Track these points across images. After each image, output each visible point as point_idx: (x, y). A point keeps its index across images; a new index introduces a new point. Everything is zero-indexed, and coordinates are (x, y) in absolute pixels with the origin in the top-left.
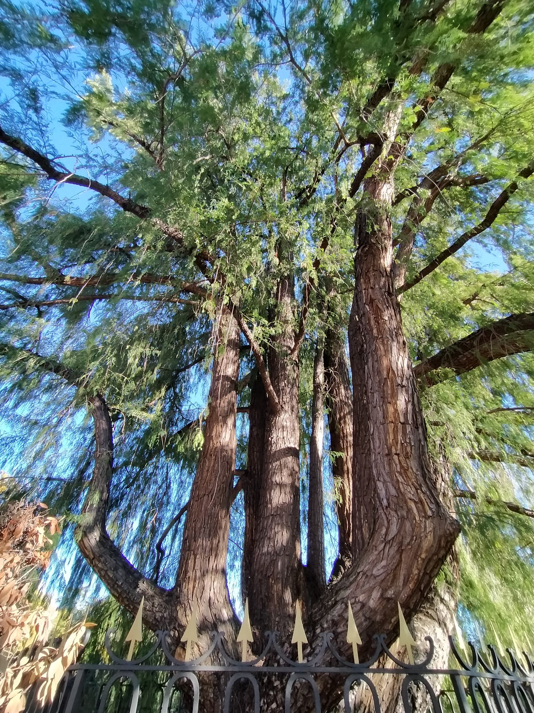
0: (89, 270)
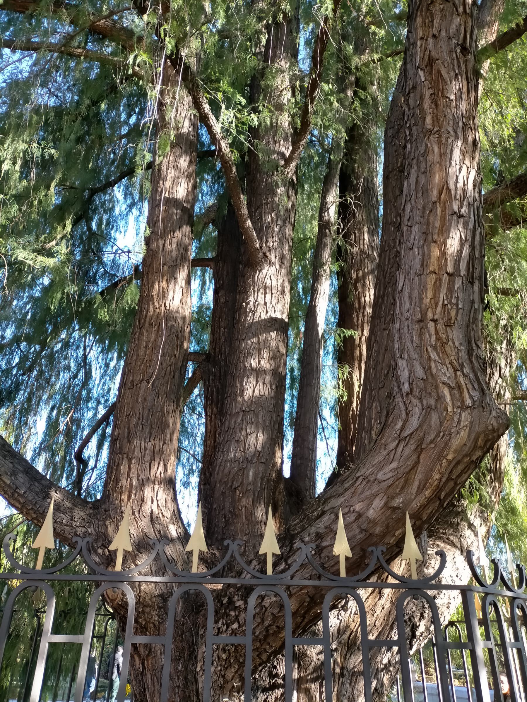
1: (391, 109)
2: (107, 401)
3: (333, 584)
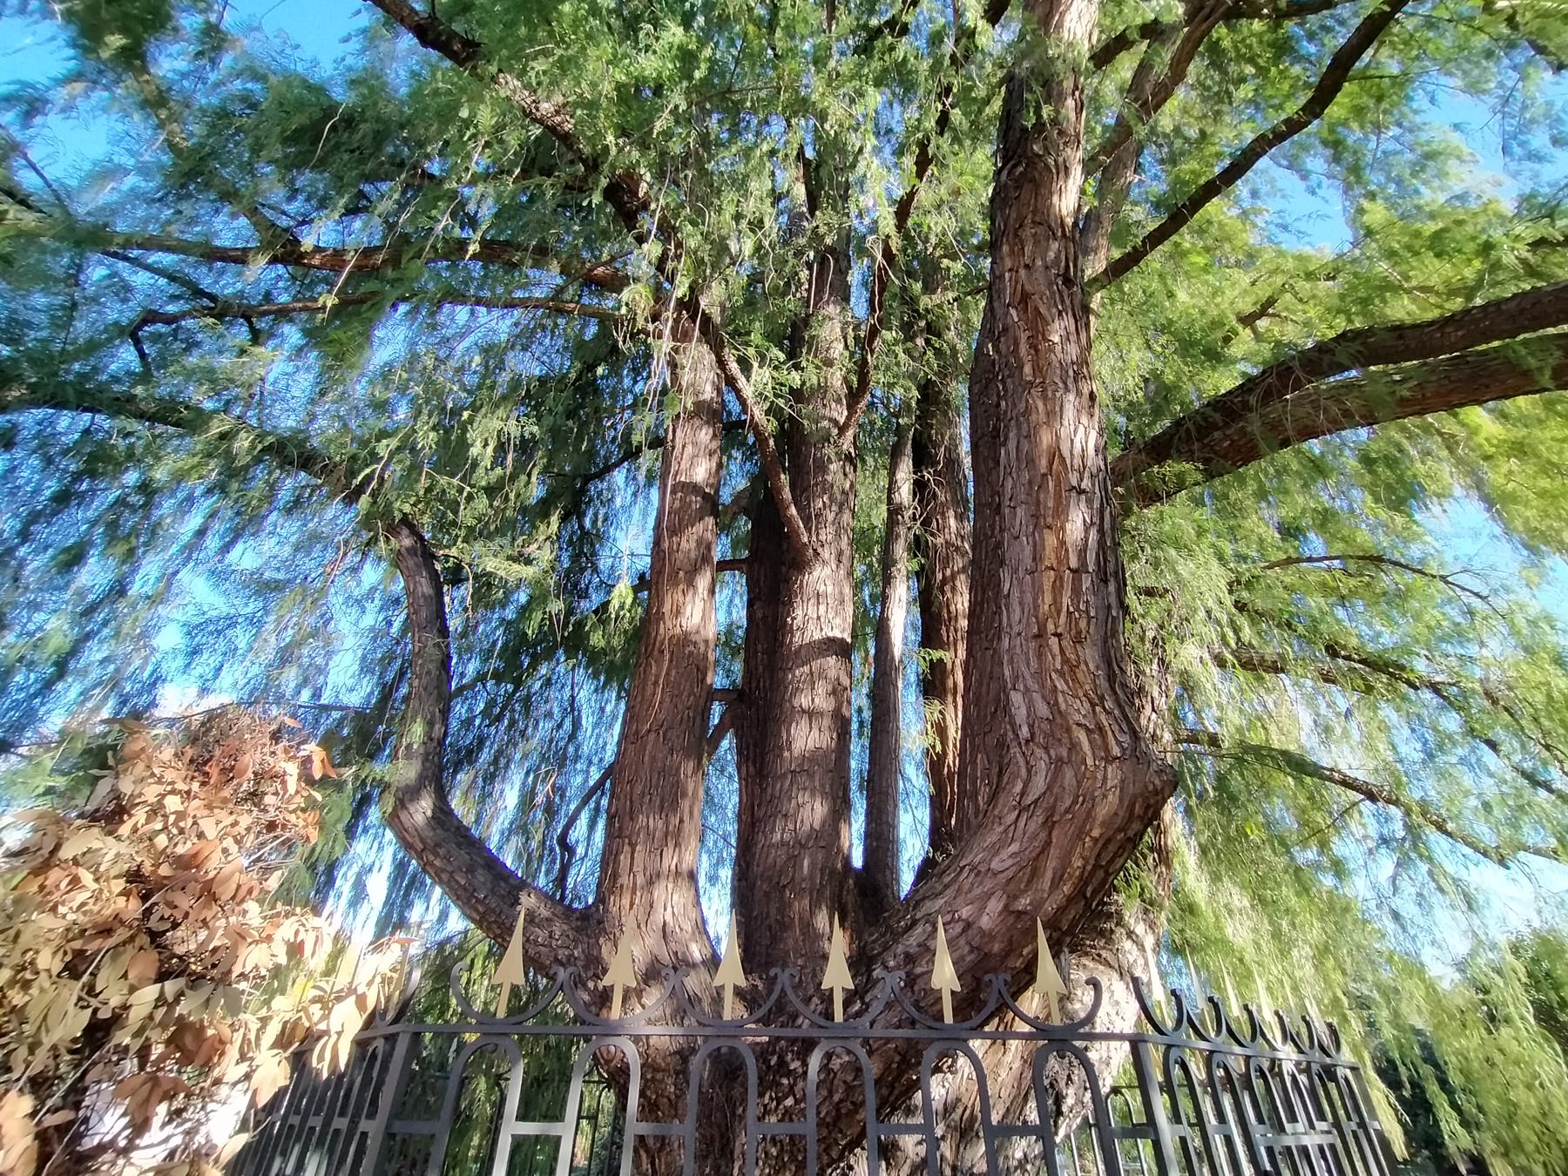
0: (363, 232)
1: (976, 358)
2: (601, 760)
3: (934, 1034)
